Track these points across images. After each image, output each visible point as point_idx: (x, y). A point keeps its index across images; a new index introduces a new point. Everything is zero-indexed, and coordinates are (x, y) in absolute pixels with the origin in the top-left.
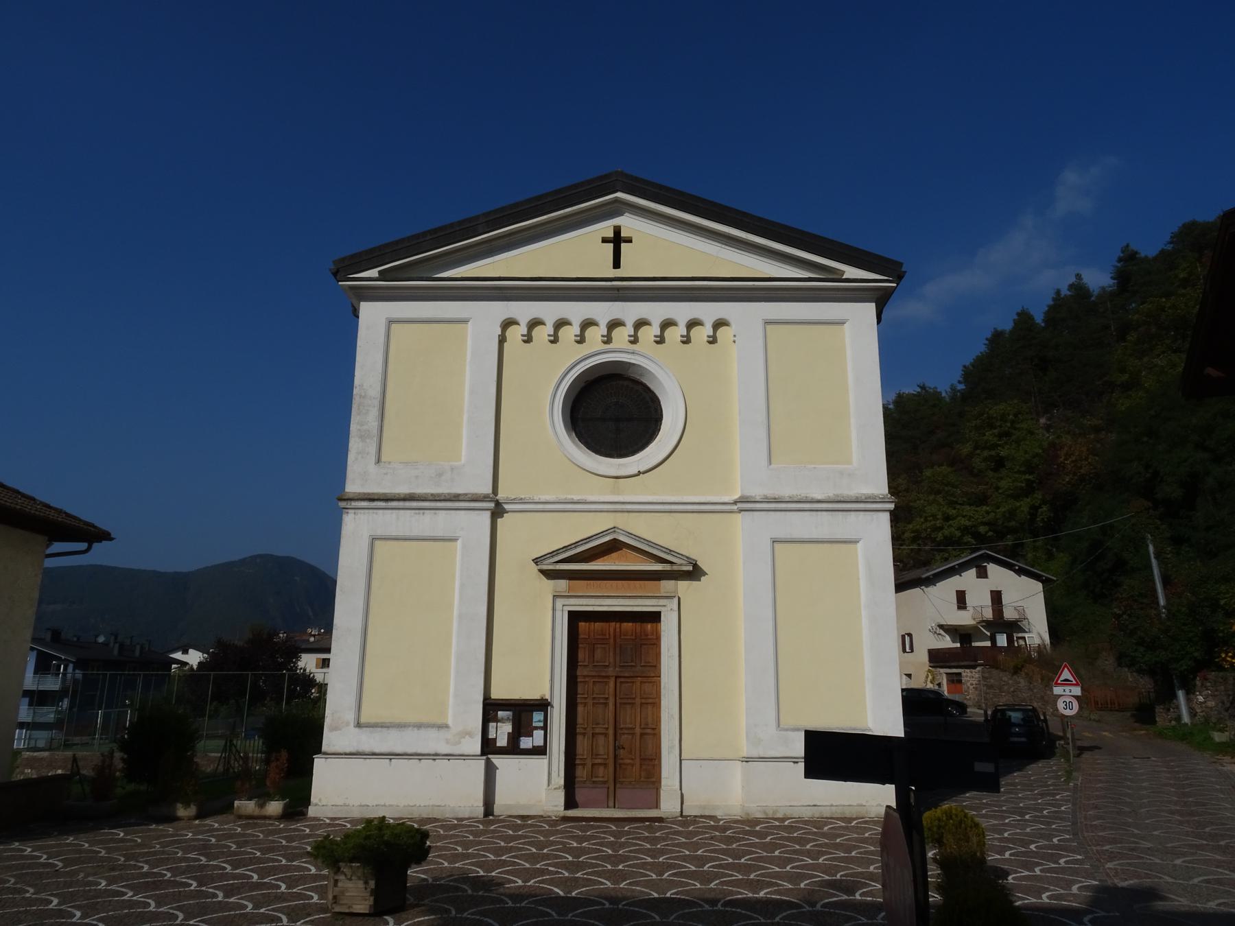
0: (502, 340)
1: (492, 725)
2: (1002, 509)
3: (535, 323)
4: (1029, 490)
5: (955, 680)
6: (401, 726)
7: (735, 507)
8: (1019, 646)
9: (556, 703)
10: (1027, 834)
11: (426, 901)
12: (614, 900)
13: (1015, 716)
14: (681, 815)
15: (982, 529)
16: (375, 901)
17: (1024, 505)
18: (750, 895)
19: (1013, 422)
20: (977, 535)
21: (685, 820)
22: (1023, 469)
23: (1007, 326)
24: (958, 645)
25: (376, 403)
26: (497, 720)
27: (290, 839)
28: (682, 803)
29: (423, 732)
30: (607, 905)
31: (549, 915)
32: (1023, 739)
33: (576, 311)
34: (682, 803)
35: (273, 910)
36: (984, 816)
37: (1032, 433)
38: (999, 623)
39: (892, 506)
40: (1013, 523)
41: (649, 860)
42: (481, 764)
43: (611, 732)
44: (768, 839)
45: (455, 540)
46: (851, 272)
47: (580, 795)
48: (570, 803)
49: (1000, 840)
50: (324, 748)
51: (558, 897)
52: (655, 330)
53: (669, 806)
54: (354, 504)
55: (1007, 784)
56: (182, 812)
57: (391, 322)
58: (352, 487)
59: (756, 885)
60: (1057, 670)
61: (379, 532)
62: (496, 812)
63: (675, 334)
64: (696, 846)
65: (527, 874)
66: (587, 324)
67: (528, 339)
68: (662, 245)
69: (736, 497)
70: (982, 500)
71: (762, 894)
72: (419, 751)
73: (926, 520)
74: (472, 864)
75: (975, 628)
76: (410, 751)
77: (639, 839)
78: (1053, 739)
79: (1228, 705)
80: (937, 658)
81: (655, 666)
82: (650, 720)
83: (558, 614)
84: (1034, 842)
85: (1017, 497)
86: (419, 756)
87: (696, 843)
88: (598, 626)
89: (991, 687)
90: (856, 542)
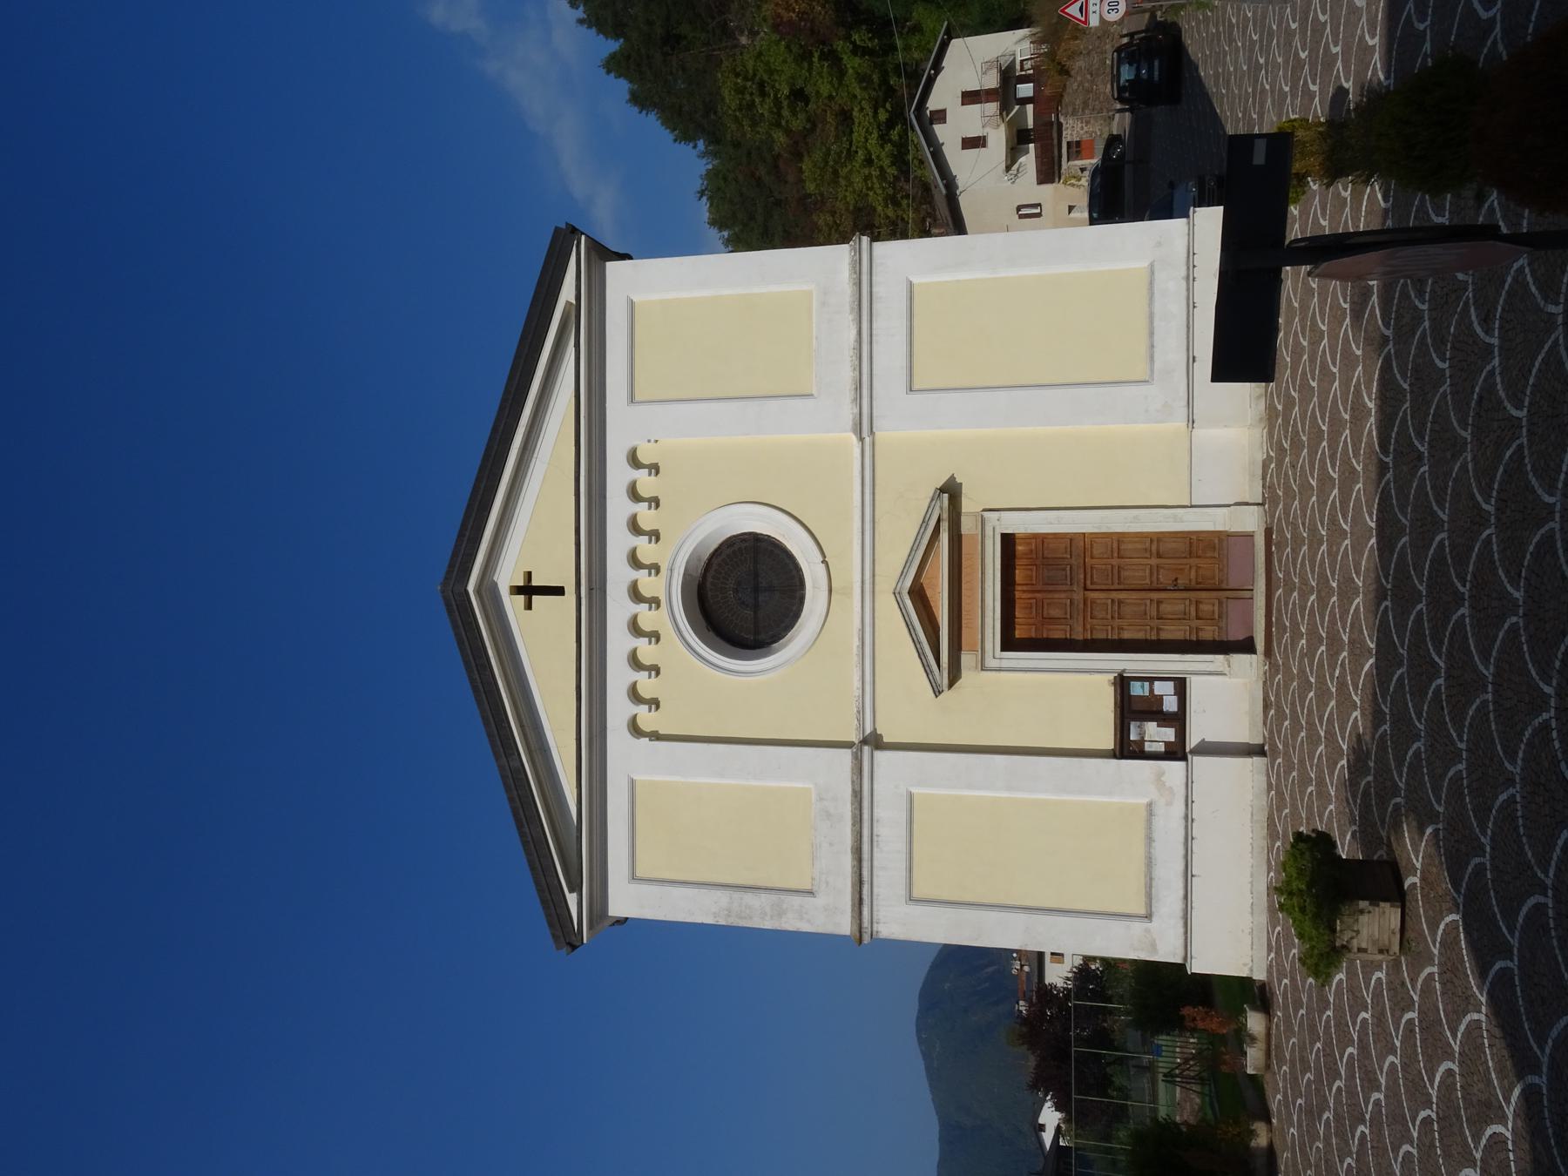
0: (656, 736)
1: (1148, 747)
2: (858, 92)
3: (634, 695)
4: (832, 57)
5: (1077, 149)
6: (1149, 863)
7: (867, 440)
8: (1033, 68)
9: (1120, 666)
10: (1286, 62)
11: (1384, 834)
12: (1381, 595)
13: (1127, 73)
14: (1262, 505)
15: (883, 116)
16: (1385, 900)
17: (852, 63)
18: (1372, 419)
19: (746, 79)
20: (890, 124)
21: (1269, 500)
22: (806, 65)
23: (623, 87)
24: (1032, 146)
25: (737, 895)
26: (1142, 742)
27: (1298, 1004)
28: (1247, 504)
29: (1155, 835)
30: (1388, 603)
31: (1401, 678)
32: (1156, 63)
33: (618, 642)
34: (1247, 504)
35: (1397, 1030)
36: (1261, 116)
37: (760, 54)
38: (1004, 94)
39: (865, 239)
40: (875, 77)
41: (1324, 547)
42: (1197, 761)
43: (1155, 595)
44: (1295, 395)
45: (911, 796)
46: (567, 293)
47: (1236, 634)
48: (1247, 646)
49: (1294, 96)
50: (1179, 960)
51: (1377, 665)
52: (642, 542)
53: (1250, 521)
54: (866, 923)
55: (1217, 84)
56: (1261, 1140)
57: (633, 877)
58: (845, 927)
59: (1359, 413)
60: (1064, 21)
61: (902, 892)
62: (1259, 741)
63: (647, 517)
64: (1305, 488)
65: (1345, 704)
66: (635, 628)
67: (655, 703)
68: (534, 532)
69: (854, 439)
70: (845, 117)
71: (1371, 405)
72: (1182, 839)
73: (871, 189)
74: (1331, 774)
75: (1010, 124)
76: (1181, 852)
77: (1295, 560)
78: (1156, 26)
80: (1048, 172)
81: (1071, 539)
82: (1139, 546)
83: (1005, 664)
84: (1297, 54)
85: (842, 73)
86: (1188, 839)
87: (1301, 487)
88: (1019, 613)
89: (1085, 104)
90: (911, 284)
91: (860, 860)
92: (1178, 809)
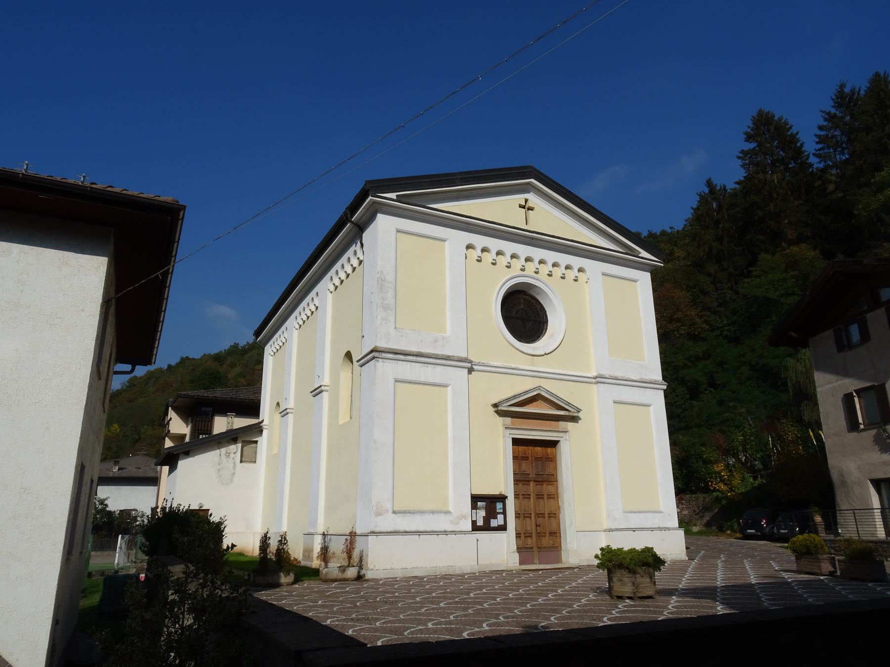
6: (422, 512)
29: (436, 515)
45: (446, 386)
54: (384, 355)
68: (550, 216)
69: (595, 374)
72: (435, 529)
76: (429, 529)
79: (698, 511)
86: (419, 533)
88: (539, 449)
90: (649, 406)
91: (417, 355)
92: (450, 528)
